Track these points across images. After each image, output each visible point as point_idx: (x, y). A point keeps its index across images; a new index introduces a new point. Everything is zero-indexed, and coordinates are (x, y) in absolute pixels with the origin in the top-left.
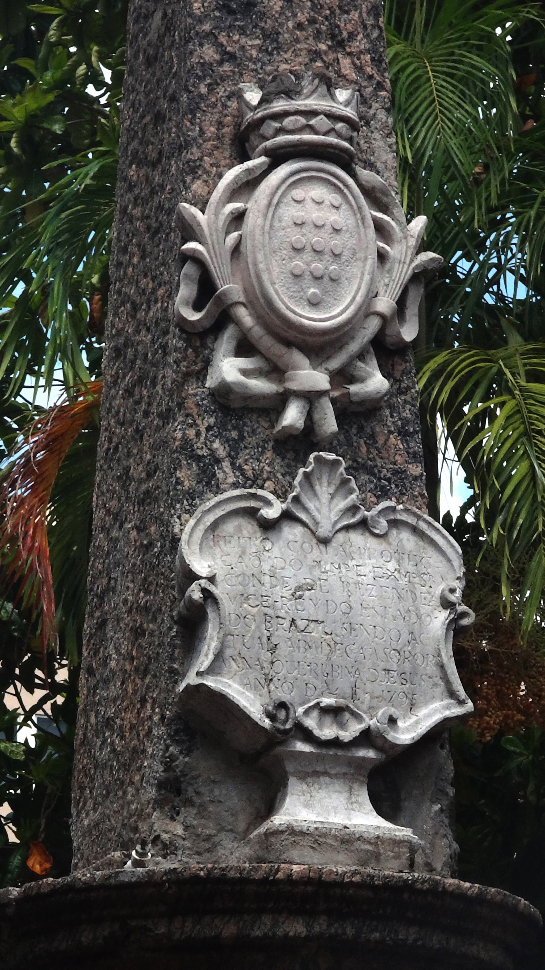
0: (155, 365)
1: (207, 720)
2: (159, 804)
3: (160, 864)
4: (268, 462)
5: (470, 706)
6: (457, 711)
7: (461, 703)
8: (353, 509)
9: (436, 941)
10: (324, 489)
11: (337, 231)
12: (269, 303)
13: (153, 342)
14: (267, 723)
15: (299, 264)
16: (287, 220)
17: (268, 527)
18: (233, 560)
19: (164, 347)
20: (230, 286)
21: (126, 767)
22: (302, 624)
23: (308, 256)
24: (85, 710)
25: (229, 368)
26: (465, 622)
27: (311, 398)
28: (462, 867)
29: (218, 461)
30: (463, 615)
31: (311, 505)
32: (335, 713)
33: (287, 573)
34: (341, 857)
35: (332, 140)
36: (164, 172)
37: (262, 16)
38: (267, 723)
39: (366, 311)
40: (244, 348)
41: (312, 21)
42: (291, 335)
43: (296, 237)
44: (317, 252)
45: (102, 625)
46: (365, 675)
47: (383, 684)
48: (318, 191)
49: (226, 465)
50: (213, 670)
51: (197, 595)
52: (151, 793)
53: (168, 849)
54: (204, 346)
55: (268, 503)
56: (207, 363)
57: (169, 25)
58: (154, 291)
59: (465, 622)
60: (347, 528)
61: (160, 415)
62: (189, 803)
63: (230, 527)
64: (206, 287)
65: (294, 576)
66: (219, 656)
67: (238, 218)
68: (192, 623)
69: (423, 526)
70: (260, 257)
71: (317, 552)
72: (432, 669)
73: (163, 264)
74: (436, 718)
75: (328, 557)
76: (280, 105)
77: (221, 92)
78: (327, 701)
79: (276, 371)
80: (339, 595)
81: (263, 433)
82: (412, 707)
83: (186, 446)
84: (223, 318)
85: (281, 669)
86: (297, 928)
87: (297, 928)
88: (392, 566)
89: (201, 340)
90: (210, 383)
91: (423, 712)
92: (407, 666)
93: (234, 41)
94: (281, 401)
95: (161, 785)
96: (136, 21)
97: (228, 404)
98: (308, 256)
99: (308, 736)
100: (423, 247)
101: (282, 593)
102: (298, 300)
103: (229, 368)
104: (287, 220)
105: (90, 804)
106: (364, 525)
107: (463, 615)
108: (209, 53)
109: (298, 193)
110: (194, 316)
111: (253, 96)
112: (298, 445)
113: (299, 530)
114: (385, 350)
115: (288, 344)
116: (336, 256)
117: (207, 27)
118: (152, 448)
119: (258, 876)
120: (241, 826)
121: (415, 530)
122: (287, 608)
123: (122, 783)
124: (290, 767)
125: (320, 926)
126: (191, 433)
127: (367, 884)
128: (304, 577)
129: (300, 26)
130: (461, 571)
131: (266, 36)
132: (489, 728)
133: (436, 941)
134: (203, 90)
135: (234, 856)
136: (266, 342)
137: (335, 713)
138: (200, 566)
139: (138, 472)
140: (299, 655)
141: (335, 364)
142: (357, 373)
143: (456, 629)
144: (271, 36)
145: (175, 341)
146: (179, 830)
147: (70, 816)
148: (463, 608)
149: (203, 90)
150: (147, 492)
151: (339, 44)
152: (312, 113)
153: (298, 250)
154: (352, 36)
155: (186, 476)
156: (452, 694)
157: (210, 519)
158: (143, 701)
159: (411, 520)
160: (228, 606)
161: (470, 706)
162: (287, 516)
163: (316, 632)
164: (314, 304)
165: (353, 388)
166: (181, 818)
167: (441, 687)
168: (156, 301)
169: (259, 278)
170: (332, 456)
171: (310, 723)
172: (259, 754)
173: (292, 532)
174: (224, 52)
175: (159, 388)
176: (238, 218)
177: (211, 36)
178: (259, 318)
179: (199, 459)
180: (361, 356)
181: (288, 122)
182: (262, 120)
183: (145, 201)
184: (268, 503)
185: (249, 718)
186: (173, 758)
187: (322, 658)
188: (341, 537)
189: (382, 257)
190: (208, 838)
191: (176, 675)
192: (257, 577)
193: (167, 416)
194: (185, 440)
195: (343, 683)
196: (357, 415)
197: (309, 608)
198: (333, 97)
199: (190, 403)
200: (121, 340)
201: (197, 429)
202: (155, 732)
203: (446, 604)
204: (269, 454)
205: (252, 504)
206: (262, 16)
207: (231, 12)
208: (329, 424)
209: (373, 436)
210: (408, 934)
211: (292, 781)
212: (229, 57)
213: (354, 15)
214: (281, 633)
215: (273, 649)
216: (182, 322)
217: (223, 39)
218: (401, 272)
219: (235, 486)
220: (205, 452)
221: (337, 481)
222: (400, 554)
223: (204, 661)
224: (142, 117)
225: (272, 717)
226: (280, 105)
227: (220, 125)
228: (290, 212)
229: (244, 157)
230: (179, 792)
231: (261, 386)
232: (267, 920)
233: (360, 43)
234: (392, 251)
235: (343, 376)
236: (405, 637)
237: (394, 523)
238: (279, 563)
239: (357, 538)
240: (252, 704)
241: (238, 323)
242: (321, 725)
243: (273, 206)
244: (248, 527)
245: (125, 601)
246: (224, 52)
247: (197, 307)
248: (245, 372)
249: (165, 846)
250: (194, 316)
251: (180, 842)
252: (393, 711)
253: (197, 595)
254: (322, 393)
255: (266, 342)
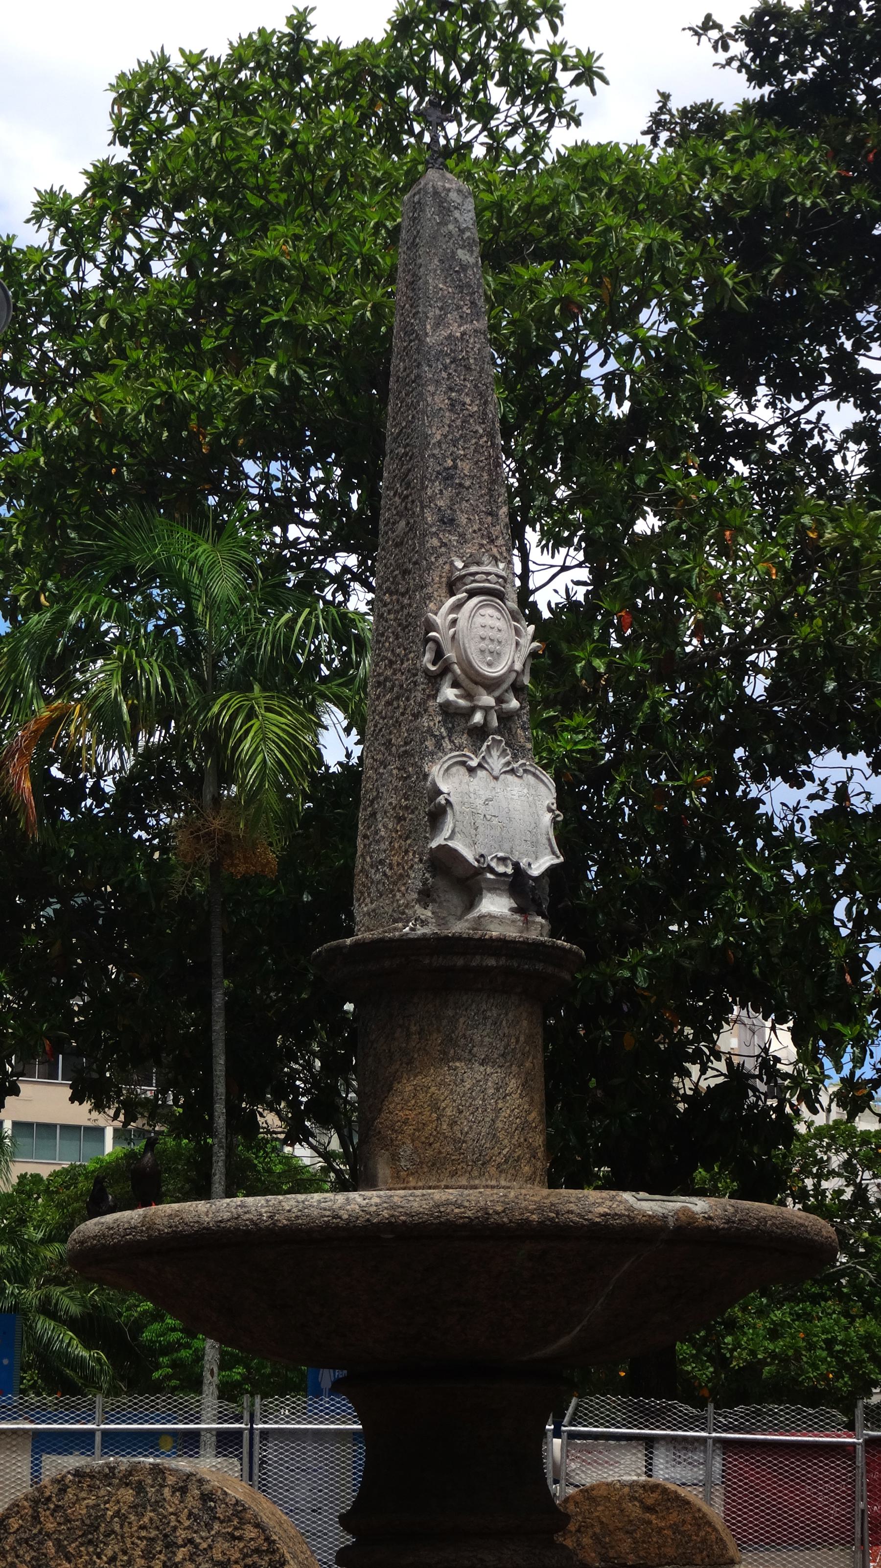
0: (410, 691)
1: (445, 863)
2: (418, 901)
3: (421, 931)
4: (464, 739)
5: (562, 859)
6: (556, 861)
7: (558, 857)
8: (508, 764)
9: (550, 970)
10: (495, 753)
11: (500, 630)
12: (470, 663)
13: (406, 679)
14: (476, 864)
15: (483, 645)
16: (477, 625)
17: (471, 770)
18: (457, 785)
19: (415, 683)
20: (450, 654)
21: (395, 883)
22: (488, 817)
23: (487, 642)
24: (362, 855)
25: (449, 693)
26: (559, 819)
27: (486, 710)
28: (553, 934)
29: (443, 738)
30: (558, 816)
31: (489, 760)
32: (503, 860)
33: (481, 792)
34: (512, 929)
35: (498, 587)
36: (410, 598)
37: (458, 526)
38: (476, 864)
39: (511, 670)
40: (455, 684)
41: (480, 530)
42: (478, 679)
43: (482, 632)
44: (492, 640)
45: (373, 815)
46: (517, 842)
47: (525, 847)
48: (490, 611)
49: (447, 740)
50: (451, 838)
51: (443, 802)
52: (416, 896)
53: (424, 923)
54: (436, 682)
55: (471, 759)
56: (438, 690)
57: (411, 528)
58: (406, 655)
59: (559, 819)
60: (505, 772)
61: (413, 715)
62: (434, 901)
63: (454, 770)
64: (439, 654)
65: (485, 794)
66: (453, 832)
67: (454, 622)
68: (437, 815)
69: (538, 773)
70: (466, 641)
71: (493, 783)
72: (545, 841)
73: (413, 642)
74: (547, 865)
75: (498, 785)
76: (474, 569)
77: (441, 561)
78: (500, 854)
79: (469, 696)
80: (504, 804)
81: (463, 726)
82: (536, 858)
83: (430, 730)
84: (447, 669)
85: (480, 838)
86: (492, 962)
87: (492, 962)
88: (525, 791)
89: (434, 680)
90: (439, 700)
91: (542, 861)
92: (534, 839)
93: (447, 537)
94: (473, 710)
95: (420, 892)
96: (386, 525)
97: (448, 711)
98: (487, 642)
99: (492, 870)
100: (533, 640)
101: (479, 802)
102: (483, 663)
103: (449, 693)
104: (477, 625)
105: (368, 900)
106: (512, 771)
107: (558, 816)
108: (435, 542)
109: (482, 611)
110: (433, 668)
111: (459, 564)
112: (479, 734)
113: (484, 772)
114: (517, 689)
115: (476, 683)
116: (500, 642)
117: (434, 530)
118: (407, 730)
119: (477, 937)
120: (459, 913)
121: (534, 775)
122: (481, 809)
123: (392, 891)
124: (483, 885)
125: (503, 961)
126: (432, 724)
127: (525, 943)
128: (488, 794)
129: (474, 532)
130: (555, 795)
131: (460, 536)
132: (239, 872)
133: (550, 970)
134: (433, 560)
135: (459, 927)
136: (466, 682)
137: (503, 860)
138: (444, 788)
139: (397, 741)
140: (487, 832)
141: (497, 693)
142: (506, 699)
143: (554, 821)
144: (462, 535)
145: (420, 679)
146: (430, 914)
147: (352, 905)
148: (557, 812)
149: (433, 560)
150: (405, 752)
151: (492, 541)
152: (489, 574)
153: (483, 639)
154: (497, 537)
155: (430, 744)
156: (554, 853)
157: (446, 766)
158: (406, 852)
159: (533, 770)
160: (456, 807)
161: (562, 859)
162: (480, 765)
163: (495, 821)
164: (490, 665)
165: (504, 706)
166: (430, 908)
167: (549, 850)
168: (408, 660)
169: (465, 651)
170: (499, 738)
171: (493, 864)
172: (468, 879)
173: (481, 773)
174: (442, 543)
175: (412, 702)
176: (454, 622)
177: (436, 534)
178: (462, 670)
179: (435, 736)
180: (506, 691)
181: (477, 577)
182: (465, 576)
183: (397, 612)
184: (471, 759)
185: (467, 861)
186: (427, 879)
187: (498, 834)
188: (503, 776)
189: (517, 644)
190: (444, 918)
191: (427, 840)
192: (468, 794)
193: (416, 716)
194: (429, 727)
195: (507, 846)
196: (506, 718)
197: (491, 810)
198: (497, 566)
199: (430, 709)
200: (382, 678)
201: (433, 722)
202: (416, 866)
203: (550, 810)
204: (465, 736)
205: (464, 759)
206: (458, 526)
207: (444, 523)
208: (495, 723)
209: (510, 729)
210: (540, 966)
211: (484, 892)
212: (444, 545)
213: (498, 527)
214: (479, 821)
215: (476, 829)
216: (426, 671)
217: (441, 536)
218: (525, 651)
219: (451, 750)
220: (437, 733)
221: (501, 750)
222: (528, 785)
223: (446, 833)
224: (393, 571)
225: (478, 861)
226: (474, 569)
227: (441, 577)
228: (479, 620)
229: (452, 594)
230: (428, 896)
231: (462, 702)
232: (478, 957)
233: (500, 542)
234: (521, 641)
235: (500, 700)
236: (533, 825)
237: (525, 771)
238: (477, 788)
239: (510, 778)
240: (469, 855)
241: (453, 672)
242: (498, 865)
243: (472, 616)
244: (462, 770)
245: (391, 804)
246: (442, 543)
247: (434, 664)
248: (456, 696)
249: (422, 921)
250: (433, 668)
251: (430, 920)
252: (530, 860)
253: (443, 802)
254: (492, 707)
255: (466, 682)
